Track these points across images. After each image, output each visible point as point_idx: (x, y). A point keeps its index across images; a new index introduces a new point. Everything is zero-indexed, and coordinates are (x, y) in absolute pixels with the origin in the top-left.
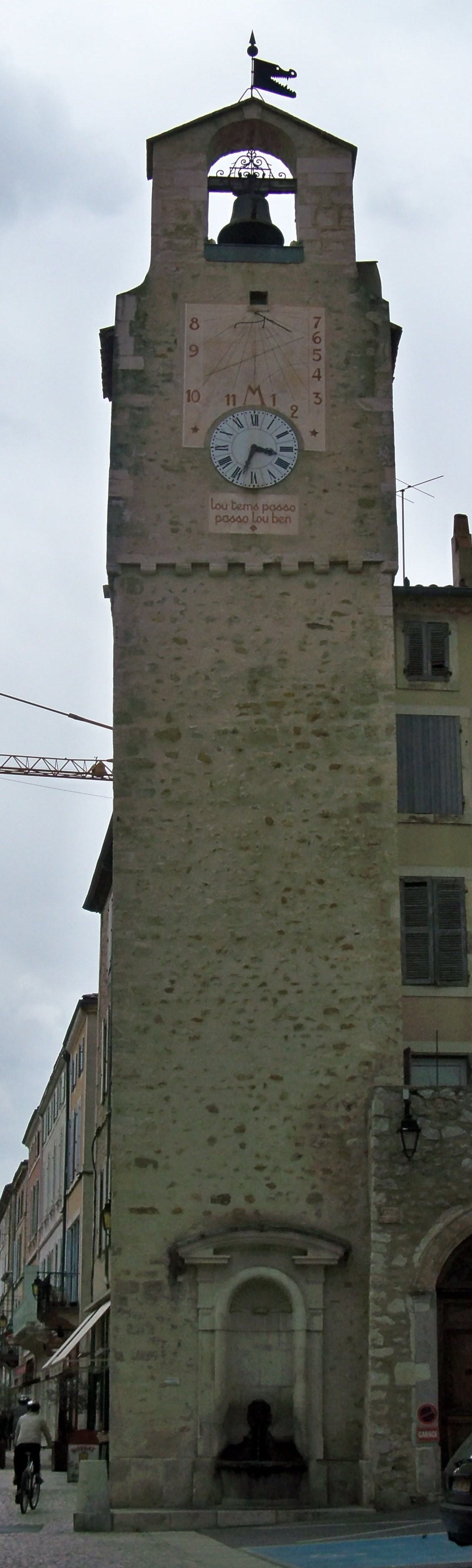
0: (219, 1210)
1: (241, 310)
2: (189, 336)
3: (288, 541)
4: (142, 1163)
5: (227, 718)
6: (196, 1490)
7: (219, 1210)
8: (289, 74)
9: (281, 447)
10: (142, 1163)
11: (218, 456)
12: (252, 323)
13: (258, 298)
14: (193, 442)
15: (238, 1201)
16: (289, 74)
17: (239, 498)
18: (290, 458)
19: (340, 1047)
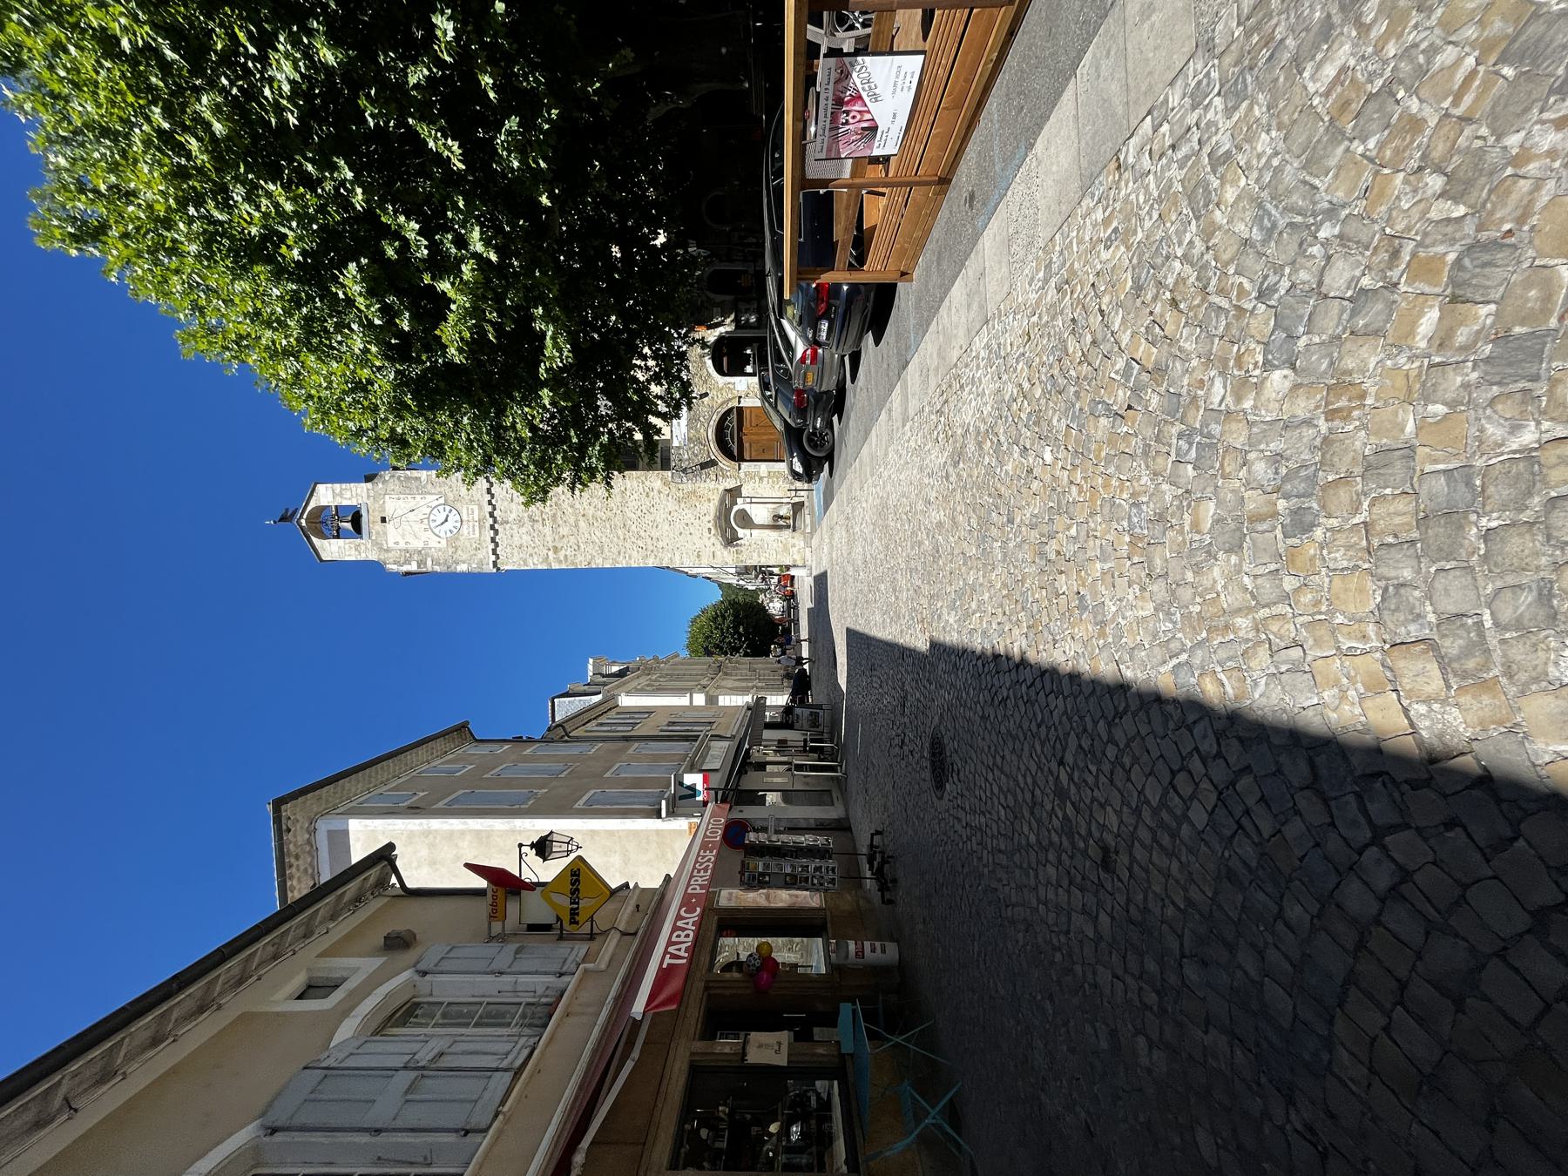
0: (713, 532)
1: (389, 526)
2: (402, 545)
3: (480, 508)
4: (698, 556)
5: (547, 530)
6: (1363, 685)
7: (713, 532)
8: (287, 510)
9: (835, 1025)
10: (698, 556)
11: (449, 534)
12: (467, 1132)
13: (383, 520)
14: (444, 542)
15: (710, 525)
16: (287, 510)
17: (465, 526)
18: (448, 508)
19: (660, 492)
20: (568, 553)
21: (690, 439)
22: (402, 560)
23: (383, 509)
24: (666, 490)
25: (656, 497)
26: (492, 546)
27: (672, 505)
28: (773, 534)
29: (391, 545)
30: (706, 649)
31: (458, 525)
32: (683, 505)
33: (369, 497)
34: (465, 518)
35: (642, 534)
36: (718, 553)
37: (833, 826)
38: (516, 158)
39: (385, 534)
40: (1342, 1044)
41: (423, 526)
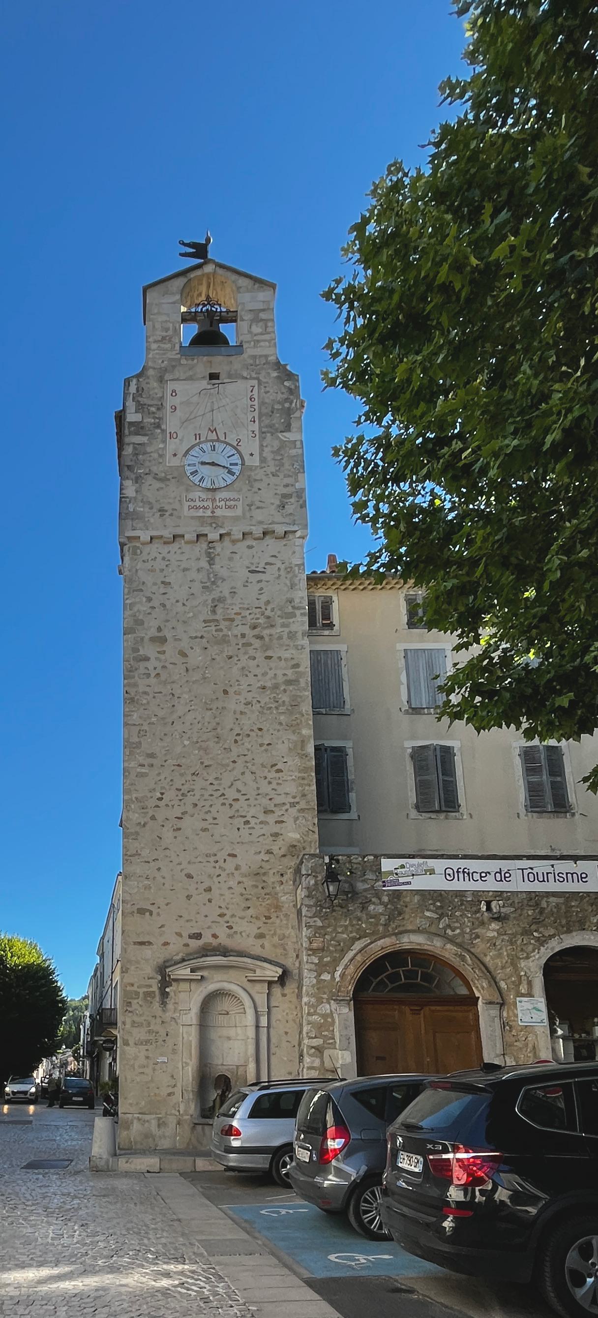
1: (204, 384)
2: (169, 401)
11: (189, 470)
14: (175, 462)
19: (276, 835)
20: (151, 665)
21: (397, 895)
22: (143, 400)
23: (234, 376)
24: (279, 847)
25: (266, 830)
26: (167, 534)
27: (248, 859)
28: (188, 1073)
29: (170, 386)
30: (301, 507)
31: (207, 484)
32: (248, 882)
33: (254, 357)
34: (219, 495)
35: (190, 800)
36: (147, 952)
37: (265, 287)
38: (511, 999)
39: (190, 378)
40: (371, 943)
41: (204, 433)
